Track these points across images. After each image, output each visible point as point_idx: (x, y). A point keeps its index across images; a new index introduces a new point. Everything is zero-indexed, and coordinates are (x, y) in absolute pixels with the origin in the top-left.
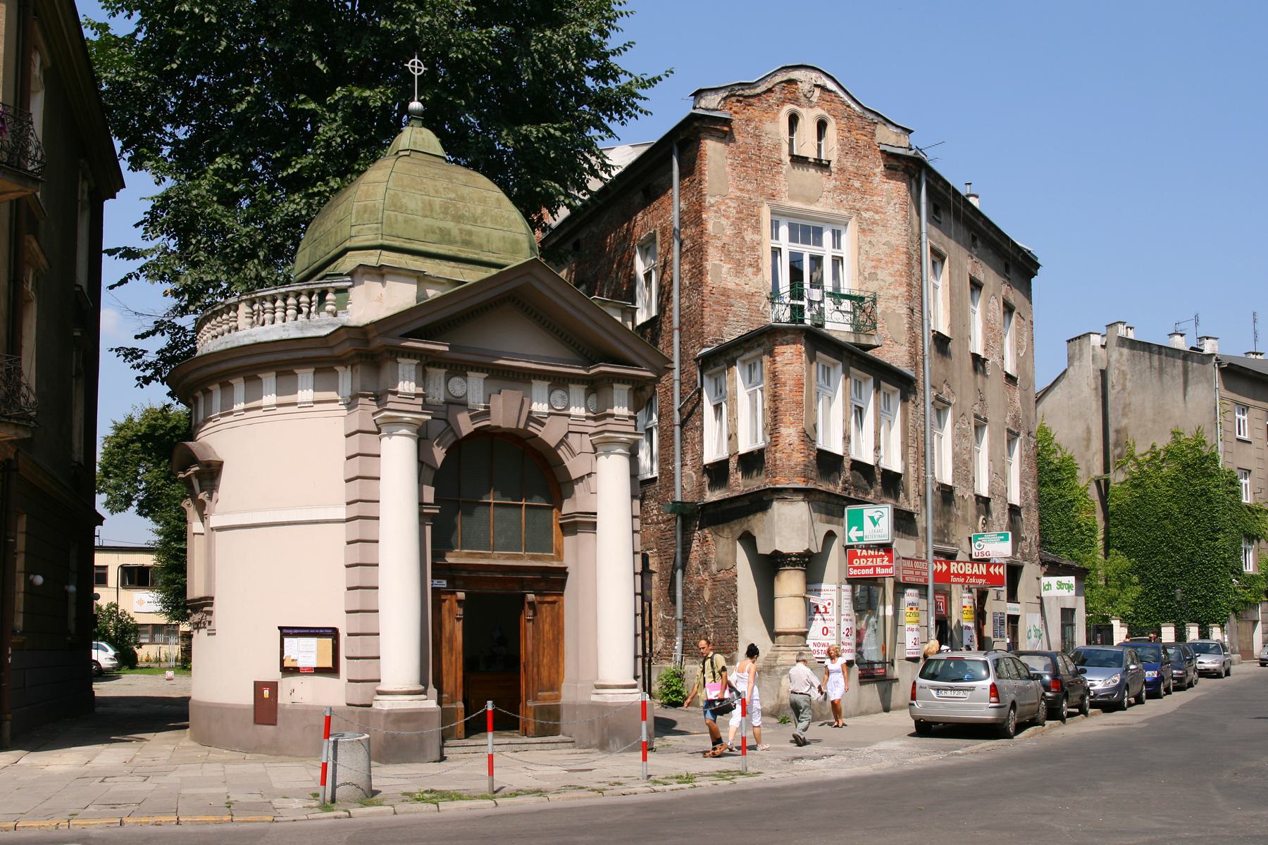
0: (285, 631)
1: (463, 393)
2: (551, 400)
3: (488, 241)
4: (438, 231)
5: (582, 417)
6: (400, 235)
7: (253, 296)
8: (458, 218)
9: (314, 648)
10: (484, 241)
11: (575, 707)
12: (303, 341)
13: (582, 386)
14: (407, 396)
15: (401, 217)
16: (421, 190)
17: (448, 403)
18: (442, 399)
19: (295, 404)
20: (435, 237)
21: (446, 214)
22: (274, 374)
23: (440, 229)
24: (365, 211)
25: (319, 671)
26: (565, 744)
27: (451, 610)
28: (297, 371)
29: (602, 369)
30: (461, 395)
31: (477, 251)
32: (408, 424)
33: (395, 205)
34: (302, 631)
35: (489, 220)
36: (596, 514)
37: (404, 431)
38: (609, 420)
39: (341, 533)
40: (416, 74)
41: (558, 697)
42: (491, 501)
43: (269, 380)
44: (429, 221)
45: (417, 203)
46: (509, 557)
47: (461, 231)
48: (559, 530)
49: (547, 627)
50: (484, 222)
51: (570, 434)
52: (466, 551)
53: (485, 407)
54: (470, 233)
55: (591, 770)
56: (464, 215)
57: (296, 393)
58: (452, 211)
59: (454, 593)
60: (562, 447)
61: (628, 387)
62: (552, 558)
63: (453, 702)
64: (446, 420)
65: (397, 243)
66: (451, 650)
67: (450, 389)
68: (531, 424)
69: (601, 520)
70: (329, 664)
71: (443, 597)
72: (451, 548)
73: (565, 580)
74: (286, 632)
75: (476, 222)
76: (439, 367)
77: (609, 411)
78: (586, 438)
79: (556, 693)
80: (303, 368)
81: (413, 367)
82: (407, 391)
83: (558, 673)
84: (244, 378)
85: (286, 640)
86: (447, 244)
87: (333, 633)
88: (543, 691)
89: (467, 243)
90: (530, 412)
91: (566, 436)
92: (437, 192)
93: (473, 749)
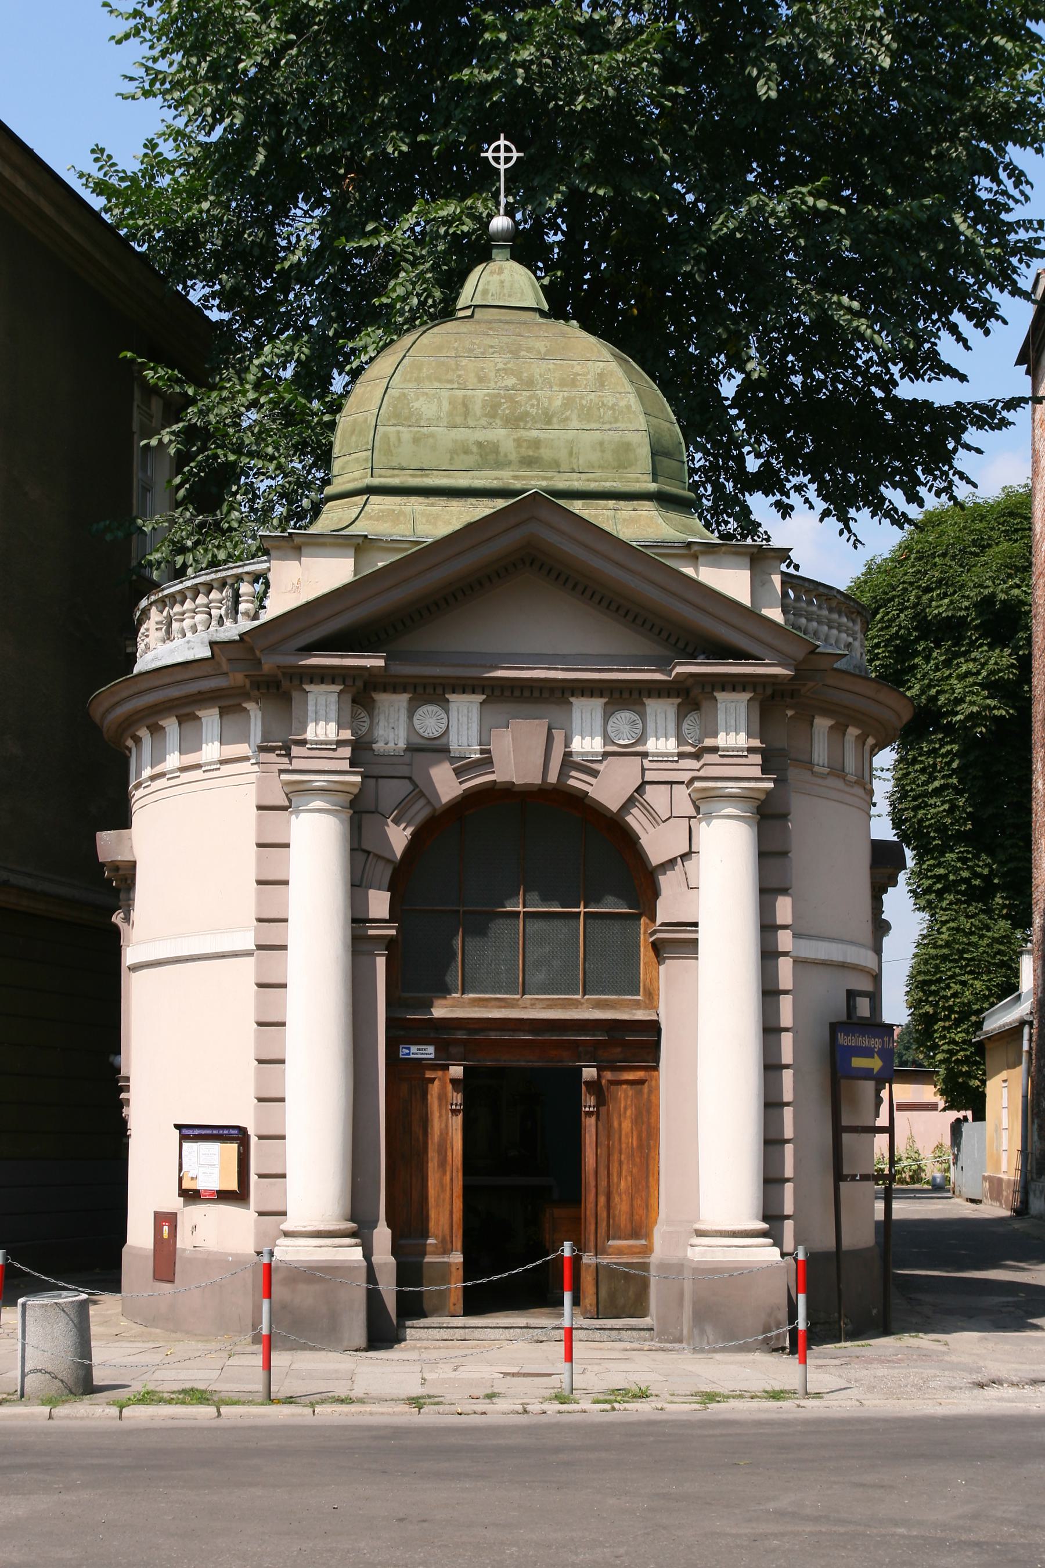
0: (185, 1131)
1: (441, 731)
2: (609, 729)
3: (571, 454)
4: (475, 449)
5: (672, 755)
6: (404, 465)
7: (160, 595)
8: (514, 421)
9: (216, 1160)
10: (563, 455)
11: (675, 1270)
12: (195, 664)
13: (670, 700)
14: (323, 746)
15: (406, 433)
16: (451, 382)
17: (412, 749)
18: (402, 745)
19: (198, 766)
20: (470, 460)
21: (493, 416)
22: (216, 711)
23: (480, 444)
24: (353, 432)
25: (223, 1196)
26: (634, 1333)
27: (443, 1097)
28: (199, 713)
29: (680, 669)
30: (437, 734)
31: (549, 474)
32: (322, 791)
33: (397, 416)
34: (203, 1132)
35: (574, 417)
36: (696, 924)
37: (318, 804)
38: (708, 758)
39: (247, 970)
40: (502, 167)
41: (648, 1250)
42: (520, 909)
43: (210, 718)
44: (460, 434)
45: (440, 407)
46: (551, 1005)
47: (518, 442)
48: (652, 954)
49: (626, 1125)
50: (567, 419)
51: (648, 787)
52: (471, 996)
53: (482, 752)
54: (536, 444)
55: (550, 1375)
56: (527, 413)
57: (200, 749)
58: (505, 409)
59: (446, 1068)
60: (635, 811)
61: (746, 696)
62: (637, 1005)
63: (446, 1252)
64: (410, 778)
65: (395, 481)
66: (442, 1164)
67: (417, 727)
68: (573, 773)
69: (704, 935)
70: (233, 1185)
71: (429, 1075)
72: (444, 990)
73: (657, 1044)
74: (189, 1133)
75: (549, 422)
76: (395, 691)
77: (709, 742)
78: (681, 792)
79: (643, 1242)
80: (206, 709)
81: (334, 698)
82: (322, 738)
83: (647, 1206)
84: (148, 728)
85: (185, 1145)
86: (493, 469)
87: (238, 1136)
88: (620, 1238)
89: (529, 462)
90: (568, 755)
91: (640, 789)
92: (481, 380)
93: (459, 1333)
